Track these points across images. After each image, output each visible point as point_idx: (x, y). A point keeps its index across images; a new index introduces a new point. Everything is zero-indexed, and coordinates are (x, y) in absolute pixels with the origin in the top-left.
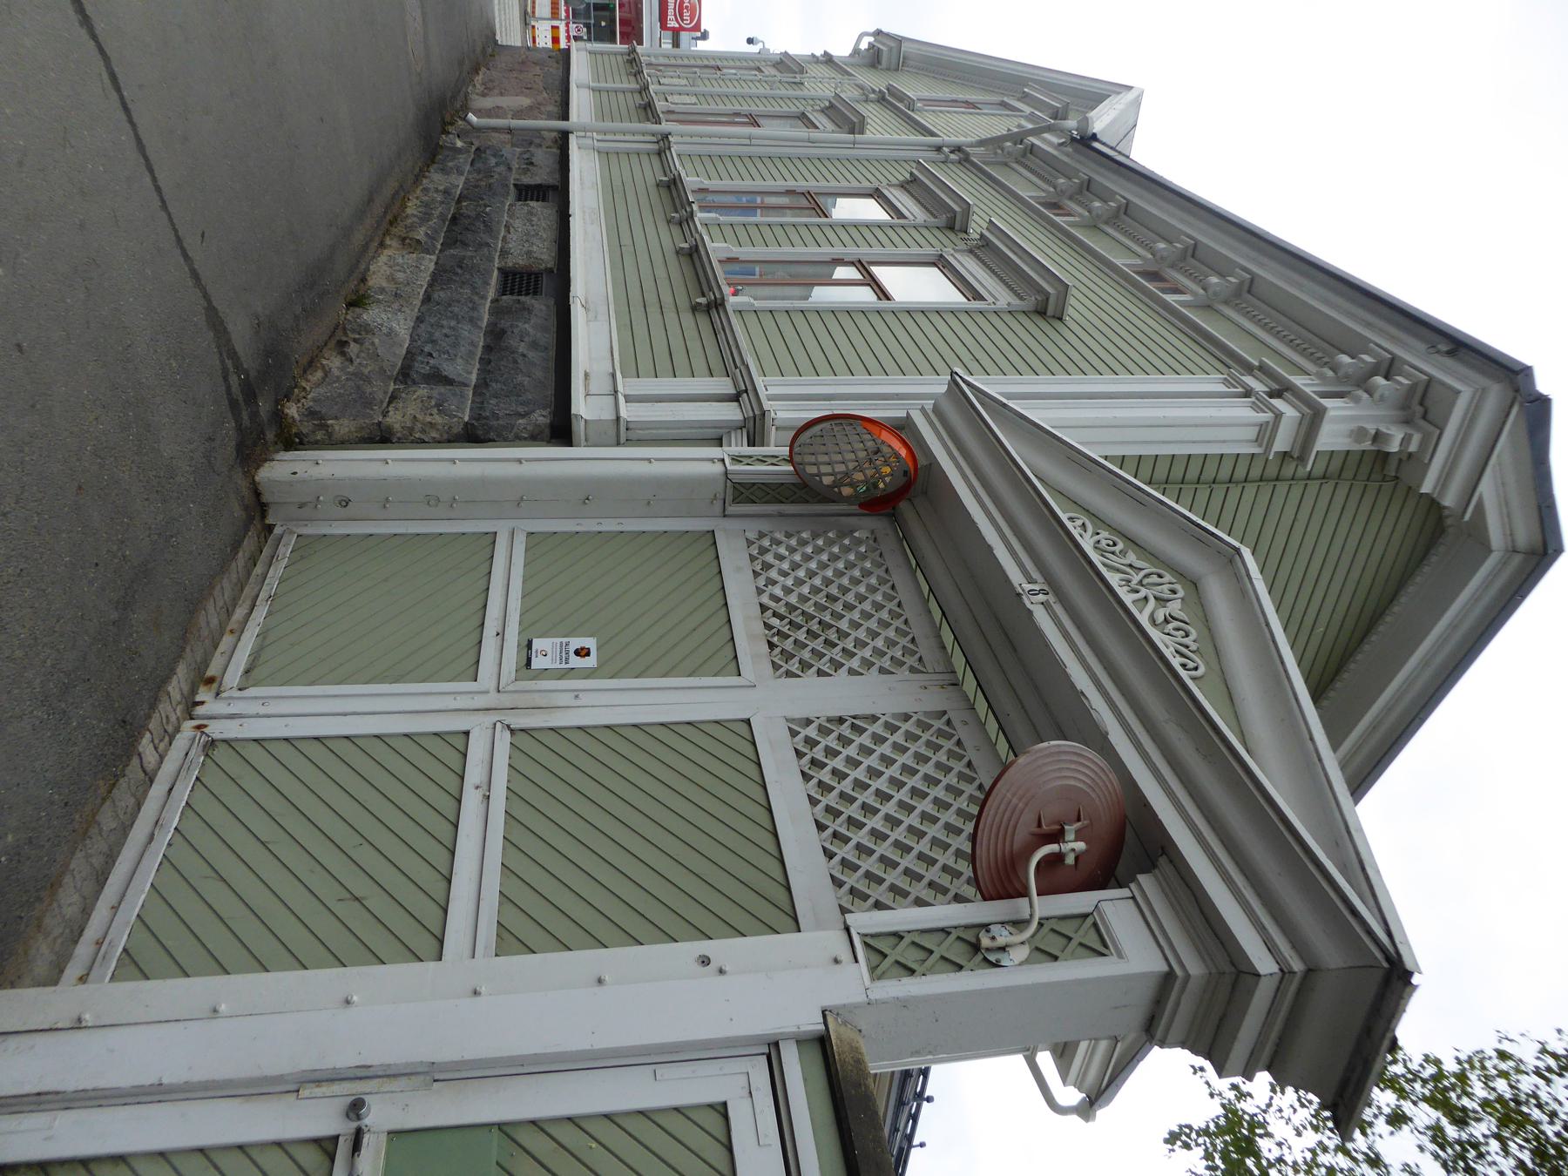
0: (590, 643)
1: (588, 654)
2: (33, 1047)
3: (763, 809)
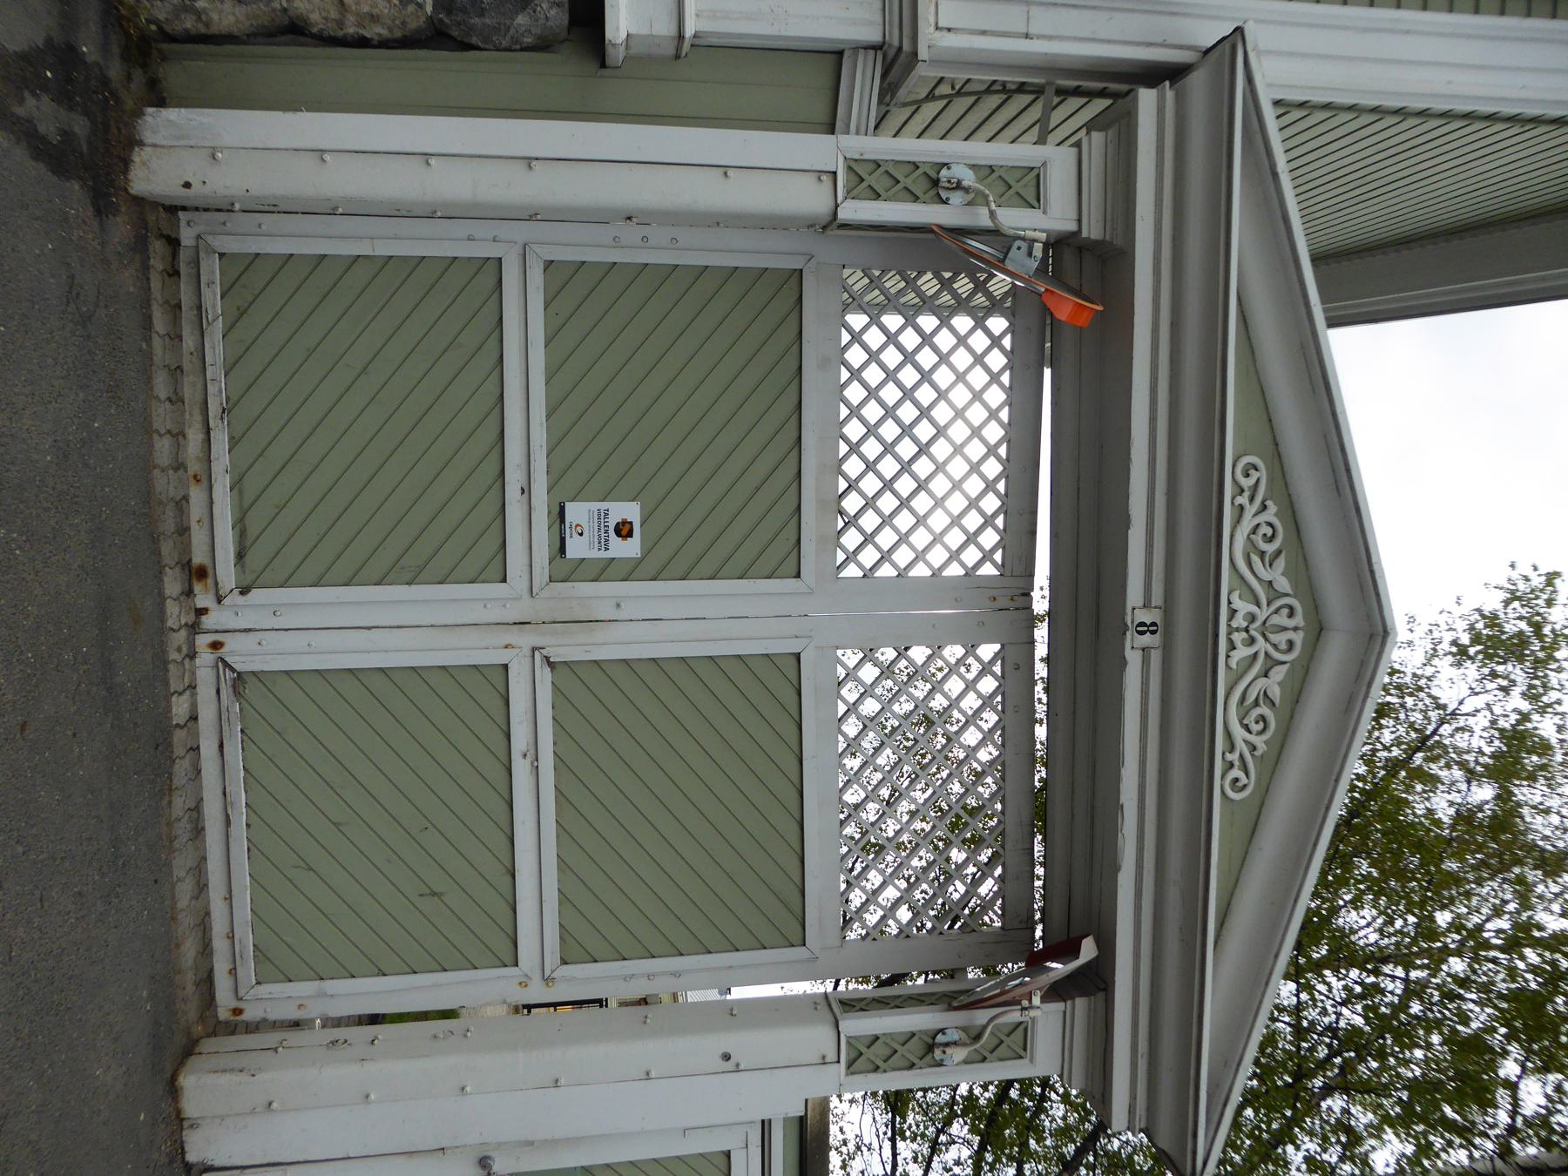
0: (630, 511)
1: (630, 534)
2: (245, 1127)
3: (793, 755)
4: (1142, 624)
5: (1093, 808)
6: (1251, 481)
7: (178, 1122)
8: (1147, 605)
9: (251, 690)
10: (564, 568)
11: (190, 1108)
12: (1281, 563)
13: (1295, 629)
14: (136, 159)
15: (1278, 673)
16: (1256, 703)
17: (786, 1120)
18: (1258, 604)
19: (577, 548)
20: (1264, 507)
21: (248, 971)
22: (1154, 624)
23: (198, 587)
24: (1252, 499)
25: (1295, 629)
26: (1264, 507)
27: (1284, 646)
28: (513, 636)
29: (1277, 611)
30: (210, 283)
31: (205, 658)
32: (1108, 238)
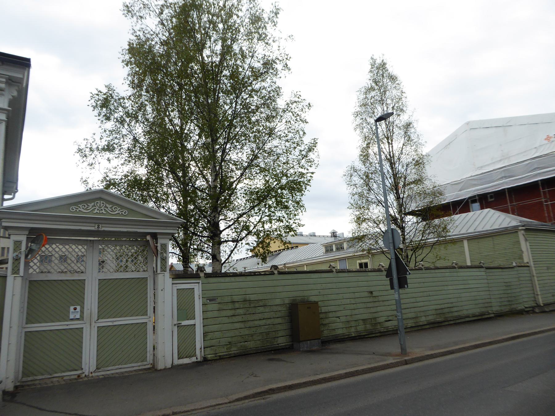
0: (72, 308)
5: (90, 329)
6: (75, 209)
7: (165, 369)
8: (95, 227)
9: (99, 367)
10: (82, 318)
11: (163, 367)
12: (89, 204)
13: (100, 202)
14: (7, 390)
15: (107, 205)
16: (112, 209)
17: (172, 281)
18: (96, 208)
19: (78, 316)
20: (79, 207)
21: (145, 363)
23: (81, 377)
24: (78, 209)
25: (100, 202)
26: (79, 207)
27: (103, 204)
28: (92, 326)
29: (97, 205)
30: (27, 379)
31: (93, 374)
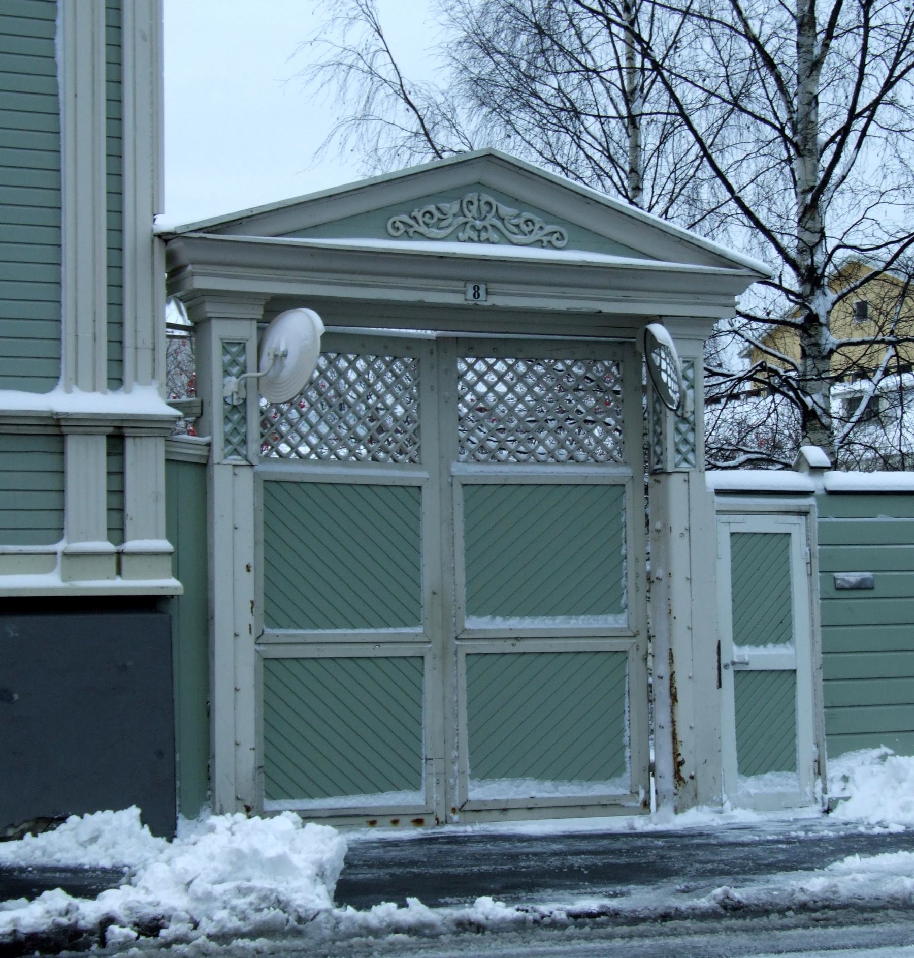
4: (474, 295)
13: (479, 200)
18: (466, 223)
22: (474, 288)
24: (411, 226)
25: (479, 200)
26: (415, 218)
32: (263, 303)
